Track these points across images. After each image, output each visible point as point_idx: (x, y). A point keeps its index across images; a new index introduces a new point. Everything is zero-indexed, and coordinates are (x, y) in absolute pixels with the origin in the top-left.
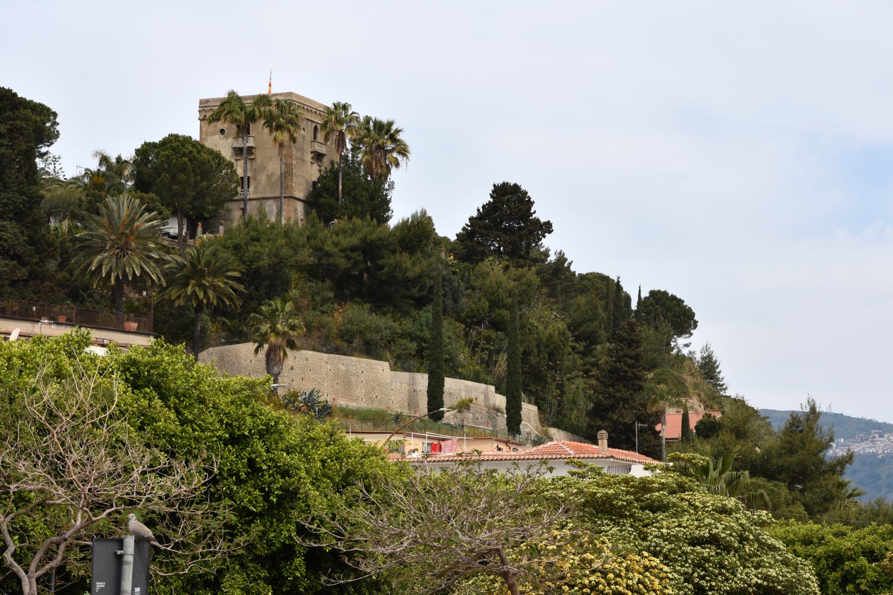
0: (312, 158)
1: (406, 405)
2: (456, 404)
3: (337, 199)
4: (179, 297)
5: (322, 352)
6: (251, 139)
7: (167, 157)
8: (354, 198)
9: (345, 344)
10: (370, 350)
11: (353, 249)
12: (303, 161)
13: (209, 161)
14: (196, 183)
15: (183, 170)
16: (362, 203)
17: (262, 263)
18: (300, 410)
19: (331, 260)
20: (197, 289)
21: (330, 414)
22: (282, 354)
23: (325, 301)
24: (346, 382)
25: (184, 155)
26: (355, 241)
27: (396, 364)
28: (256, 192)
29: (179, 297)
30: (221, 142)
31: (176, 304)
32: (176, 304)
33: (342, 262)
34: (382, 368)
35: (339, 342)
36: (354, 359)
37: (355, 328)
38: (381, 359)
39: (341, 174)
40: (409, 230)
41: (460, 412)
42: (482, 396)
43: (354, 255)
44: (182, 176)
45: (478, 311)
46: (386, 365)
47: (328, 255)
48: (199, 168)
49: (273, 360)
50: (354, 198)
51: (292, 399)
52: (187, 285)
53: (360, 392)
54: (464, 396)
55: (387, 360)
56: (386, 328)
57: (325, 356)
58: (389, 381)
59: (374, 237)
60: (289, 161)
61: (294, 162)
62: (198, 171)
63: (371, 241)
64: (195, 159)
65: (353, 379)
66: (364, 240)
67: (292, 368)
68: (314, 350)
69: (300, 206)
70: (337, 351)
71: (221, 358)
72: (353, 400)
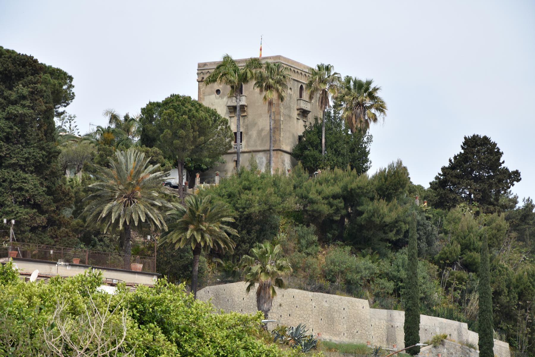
0: (298, 114)
1: (385, 339)
2: (431, 339)
3: (321, 152)
4: (179, 240)
5: (307, 290)
6: (244, 98)
7: (169, 115)
8: (336, 151)
9: (328, 283)
10: (351, 289)
11: (335, 197)
12: (290, 117)
13: (206, 119)
14: (195, 138)
15: (183, 126)
16: (343, 155)
17: (253, 210)
18: (287, 344)
19: (315, 207)
20: (195, 233)
21: (315, 348)
22: (271, 292)
23: (310, 244)
24: (329, 317)
25: (184, 113)
26: (337, 189)
27: (375, 301)
28: (247, 145)
29: (179, 240)
30: (216, 101)
31: (177, 247)
32: (177, 247)
33: (325, 209)
34: (361, 305)
35: (322, 282)
36: (336, 296)
37: (337, 269)
38: (360, 297)
39: (324, 129)
40: (386, 179)
41: (435, 347)
42: (456, 333)
43: (336, 202)
44: (182, 132)
45: (451, 253)
46: (365, 303)
47: (312, 202)
48: (198, 124)
49: (263, 297)
50: (336, 151)
51: (280, 333)
52: (186, 229)
53: (342, 327)
54: (439, 332)
55: (366, 298)
56: (365, 269)
57: (310, 294)
58: (368, 317)
59: (354, 186)
60: (277, 117)
61: (282, 119)
62: (196, 128)
63: (352, 189)
64: (194, 117)
65: (336, 315)
66: (345, 188)
67: (280, 305)
68: (300, 288)
69: (287, 158)
70: (320, 289)
71: (217, 296)
72: (335, 335)
